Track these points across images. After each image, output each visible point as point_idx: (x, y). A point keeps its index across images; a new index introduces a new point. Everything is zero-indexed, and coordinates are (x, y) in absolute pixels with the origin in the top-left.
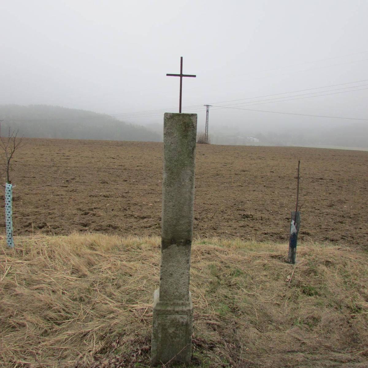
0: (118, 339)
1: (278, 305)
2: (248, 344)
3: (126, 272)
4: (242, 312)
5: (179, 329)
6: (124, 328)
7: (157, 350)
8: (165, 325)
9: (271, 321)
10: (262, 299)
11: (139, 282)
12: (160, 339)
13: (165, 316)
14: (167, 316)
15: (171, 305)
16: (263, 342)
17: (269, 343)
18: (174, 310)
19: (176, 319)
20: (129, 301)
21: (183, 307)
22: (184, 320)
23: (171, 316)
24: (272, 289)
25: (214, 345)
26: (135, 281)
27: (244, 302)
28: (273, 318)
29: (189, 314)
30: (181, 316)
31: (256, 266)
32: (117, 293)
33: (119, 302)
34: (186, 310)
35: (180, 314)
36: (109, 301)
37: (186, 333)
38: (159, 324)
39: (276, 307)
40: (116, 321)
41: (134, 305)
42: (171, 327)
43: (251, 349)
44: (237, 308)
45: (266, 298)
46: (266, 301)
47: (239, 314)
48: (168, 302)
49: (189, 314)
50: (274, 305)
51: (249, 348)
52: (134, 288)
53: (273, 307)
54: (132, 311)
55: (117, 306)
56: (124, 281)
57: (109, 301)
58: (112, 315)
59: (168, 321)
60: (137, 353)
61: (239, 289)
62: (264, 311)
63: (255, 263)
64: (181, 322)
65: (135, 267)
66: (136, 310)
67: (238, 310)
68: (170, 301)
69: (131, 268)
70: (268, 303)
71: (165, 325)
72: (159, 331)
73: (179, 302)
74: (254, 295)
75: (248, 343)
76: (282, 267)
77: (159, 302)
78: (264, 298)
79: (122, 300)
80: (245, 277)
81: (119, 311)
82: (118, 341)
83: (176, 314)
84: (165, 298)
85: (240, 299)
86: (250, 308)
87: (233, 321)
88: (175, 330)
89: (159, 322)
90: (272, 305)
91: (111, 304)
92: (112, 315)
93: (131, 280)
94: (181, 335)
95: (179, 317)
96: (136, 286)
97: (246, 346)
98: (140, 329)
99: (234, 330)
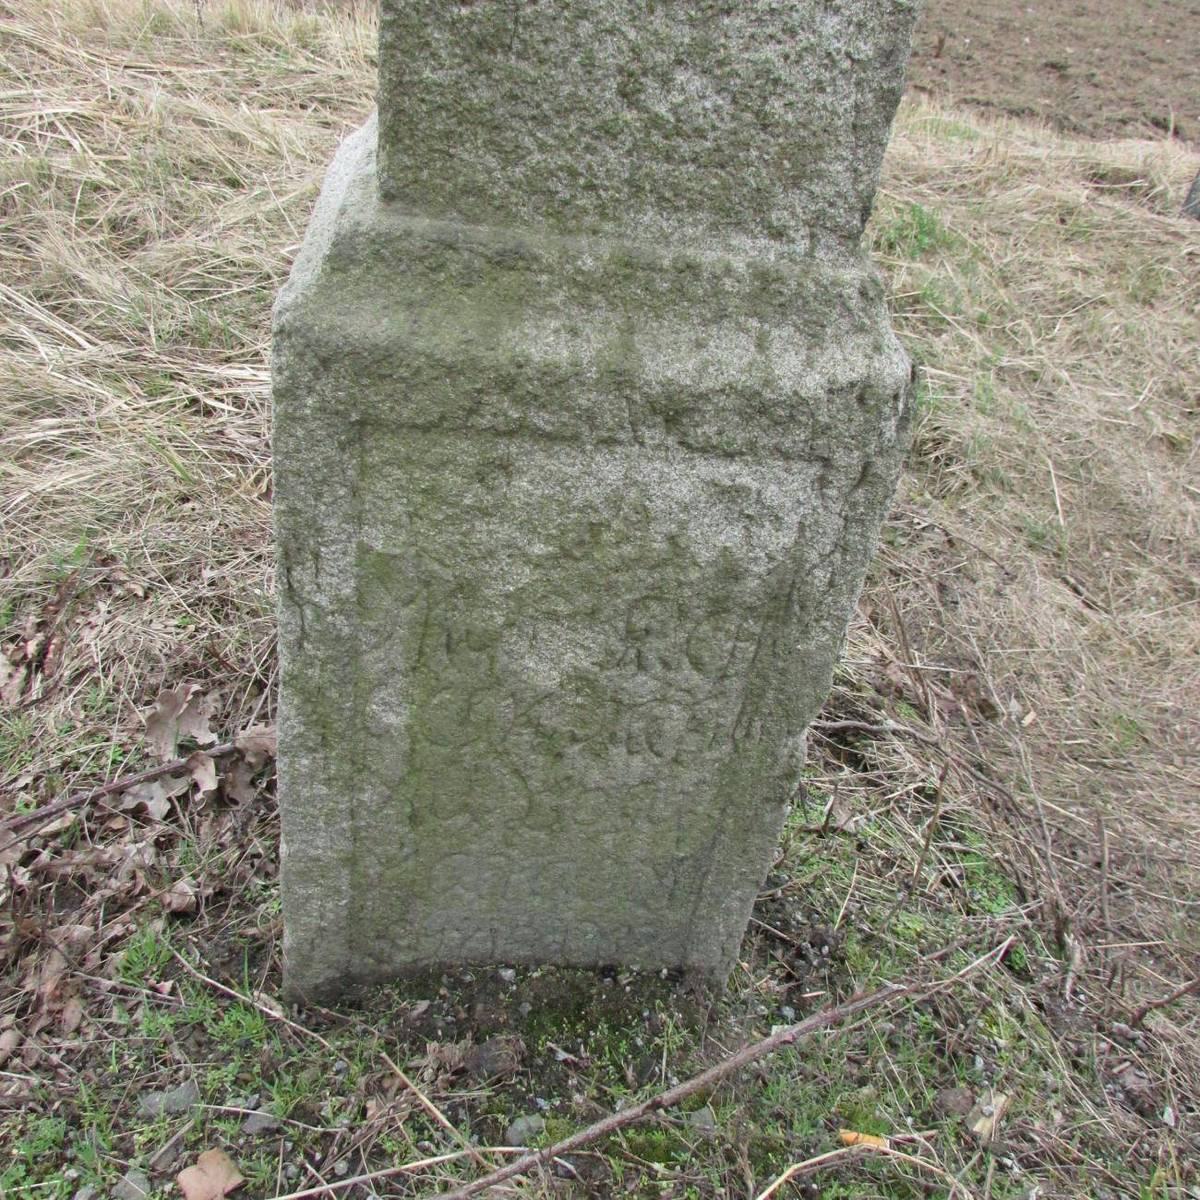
0: (41, 626)
1: (1173, 445)
2: (1034, 688)
3: (197, 154)
4: (974, 473)
5: (654, 647)
6: (112, 542)
7: (351, 861)
8: (467, 589)
9: (1140, 542)
10: (1084, 403)
11: (282, 218)
12: (389, 760)
13: (466, 450)
14: (505, 467)
15: (585, 289)
16: (1121, 678)
17: (1156, 678)
18: (619, 380)
19: (645, 516)
20: (192, 339)
21: (761, 345)
22: (765, 533)
23: (565, 463)
24: (1132, 347)
25: (863, 717)
26: (260, 216)
27: (982, 411)
28: (1152, 521)
29: (848, 460)
30: (724, 471)
31: (1025, 215)
32: (106, 280)
33: (116, 338)
34: (813, 384)
35: (706, 450)
36: (41, 329)
37: (752, 697)
38: (377, 570)
39: (1162, 457)
40: (55, 478)
41: (225, 371)
42: (553, 616)
43: (1051, 715)
44: (937, 443)
45: (1108, 401)
46: (1106, 414)
47: (956, 485)
48: (539, 239)
49: (848, 460)
50: (1149, 447)
51: (1041, 713)
52: (244, 257)
53: (1144, 459)
54: (209, 412)
55: (89, 368)
56: (178, 209)
57: (41, 329)
58: (44, 429)
59: (505, 531)
60: (180, 787)
61: (938, 333)
62: (1096, 477)
63: (1006, 198)
64: (704, 555)
65: (263, 133)
66: (238, 402)
67: (950, 460)
68: (561, 215)
69: (236, 139)
70: (1118, 428)
71: (467, 589)
72: (373, 662)
73: (709, 256)
74: (1033, 376)
75: (1034, 678)
76: (1165, 238)
77: (371, 215)
78: (1099, 399)
79: (144, 330)
80: (965, 269)
81: (101, 404)
82: (32, 648)
83: (652, 435)
84: (475, 159)
85: (952, 391)
86: (1018, 454)
87: (931, 527)
88: (611, 660)
89: (377, 539)
90: (1142, 444)
91: (44, 350)
92: (44, 429)
93: (237, 208)
94: (676, 718)
95: (683, 491)
96: (260, 250)
97: (1018, 697)
98: (243, 555)
99: (942, 588)
